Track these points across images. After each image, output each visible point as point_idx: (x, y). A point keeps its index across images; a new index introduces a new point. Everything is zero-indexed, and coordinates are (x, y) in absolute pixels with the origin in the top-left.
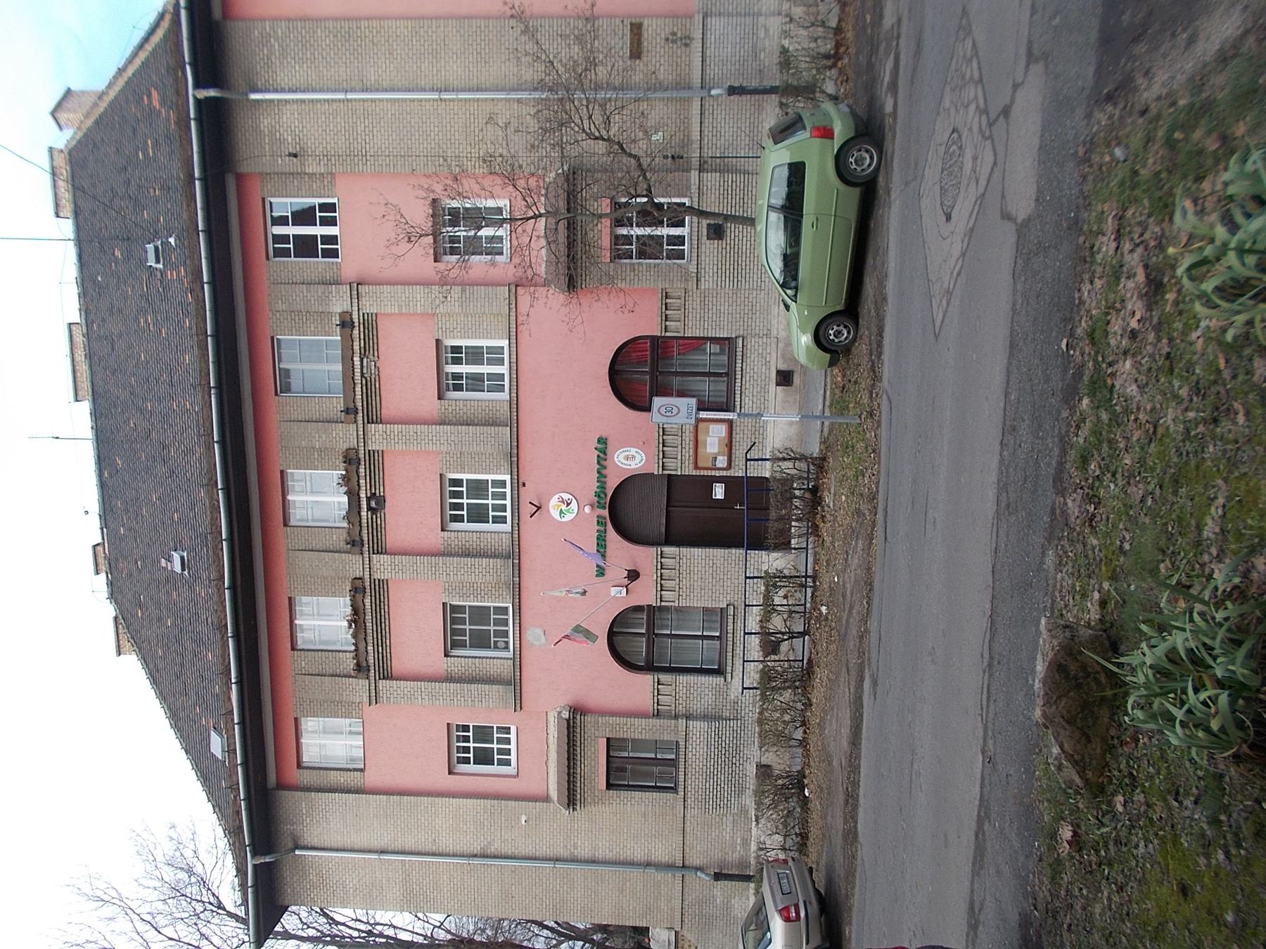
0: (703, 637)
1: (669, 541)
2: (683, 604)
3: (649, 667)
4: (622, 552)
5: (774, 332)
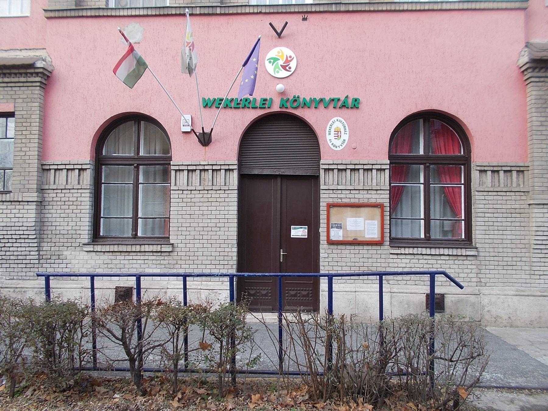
0: (135, 218)
1: (242, 177)
2: (174, 195)
3: (100, 161)
4: (230, 128)
5: (485, 290)
